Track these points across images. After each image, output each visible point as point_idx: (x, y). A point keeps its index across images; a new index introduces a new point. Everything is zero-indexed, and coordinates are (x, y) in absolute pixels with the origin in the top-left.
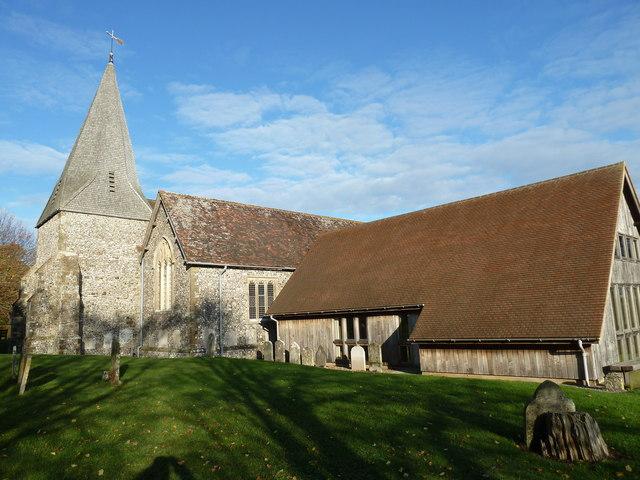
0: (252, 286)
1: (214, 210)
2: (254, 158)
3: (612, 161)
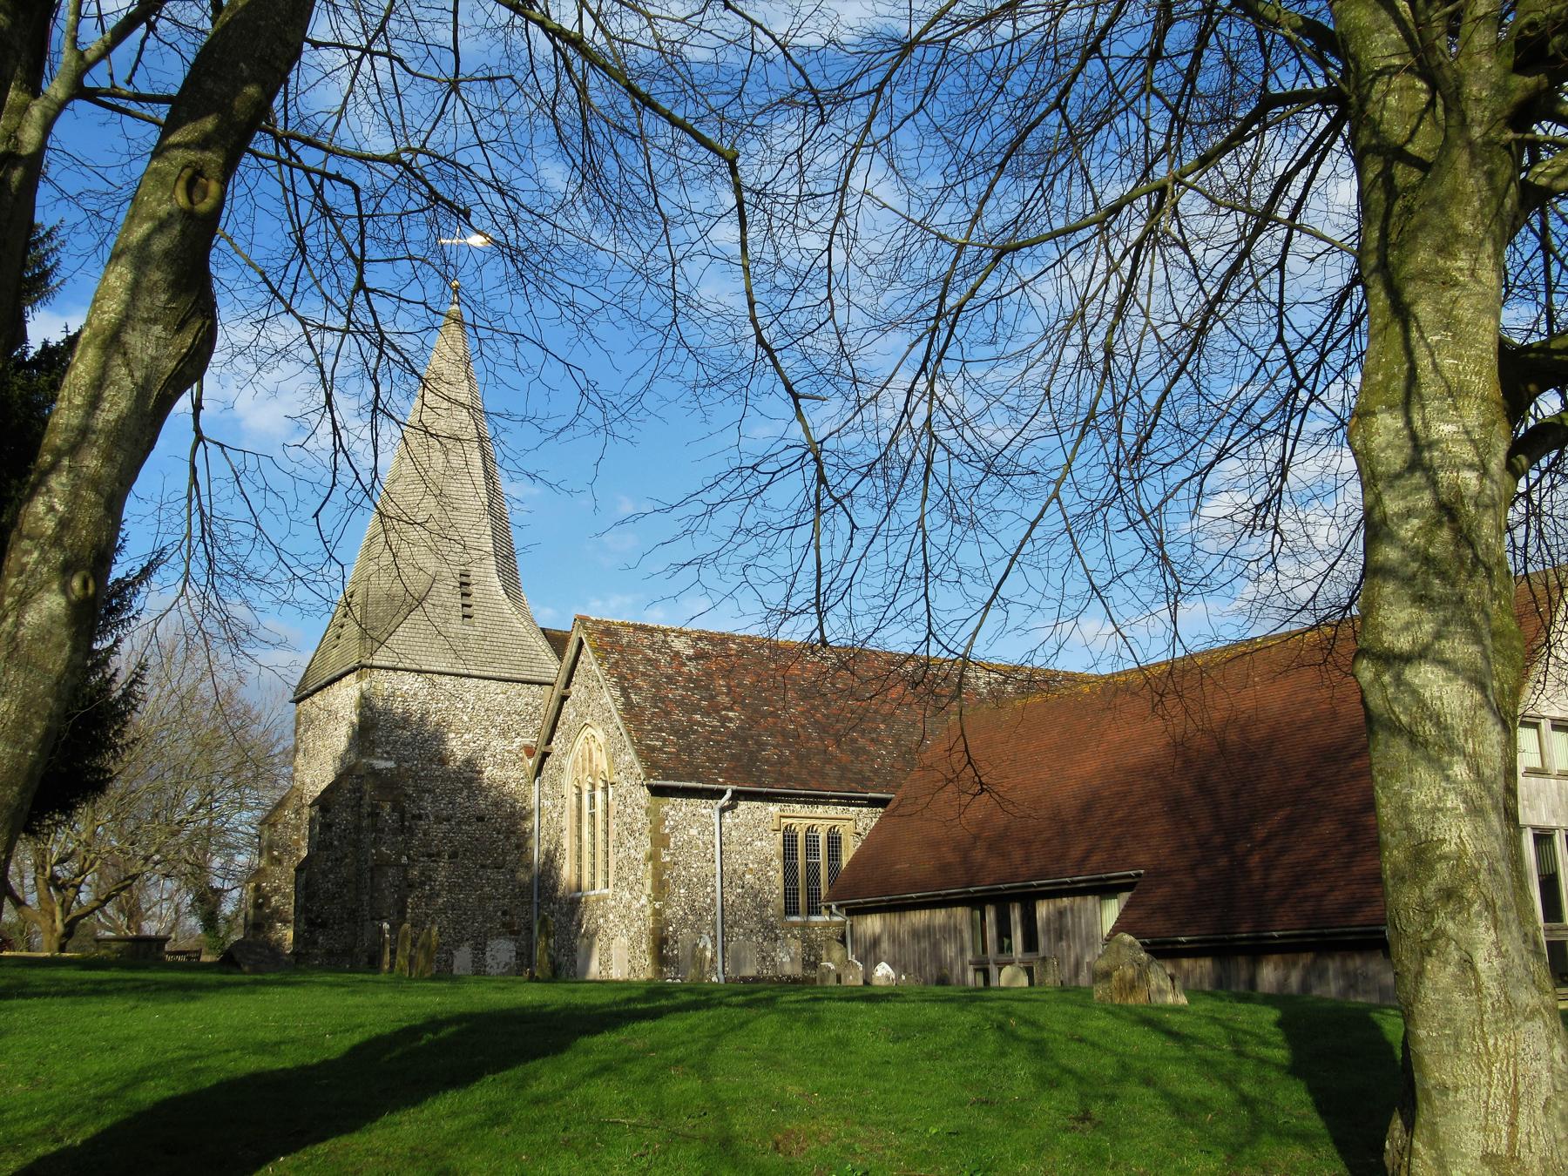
0: (789, 840)
1: (700, 656)
2: (1017, 703)
3: (1492, 357)
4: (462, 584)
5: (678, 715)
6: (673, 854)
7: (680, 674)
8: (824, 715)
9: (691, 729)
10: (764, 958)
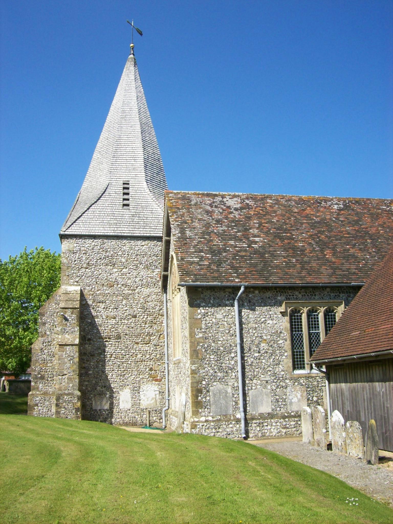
4: (124, 188)
5: (217, 242)
6: (205, 332)
7: (227, 218)
8: (327, 236)
9: (225, 249)
10: (277, 401)
